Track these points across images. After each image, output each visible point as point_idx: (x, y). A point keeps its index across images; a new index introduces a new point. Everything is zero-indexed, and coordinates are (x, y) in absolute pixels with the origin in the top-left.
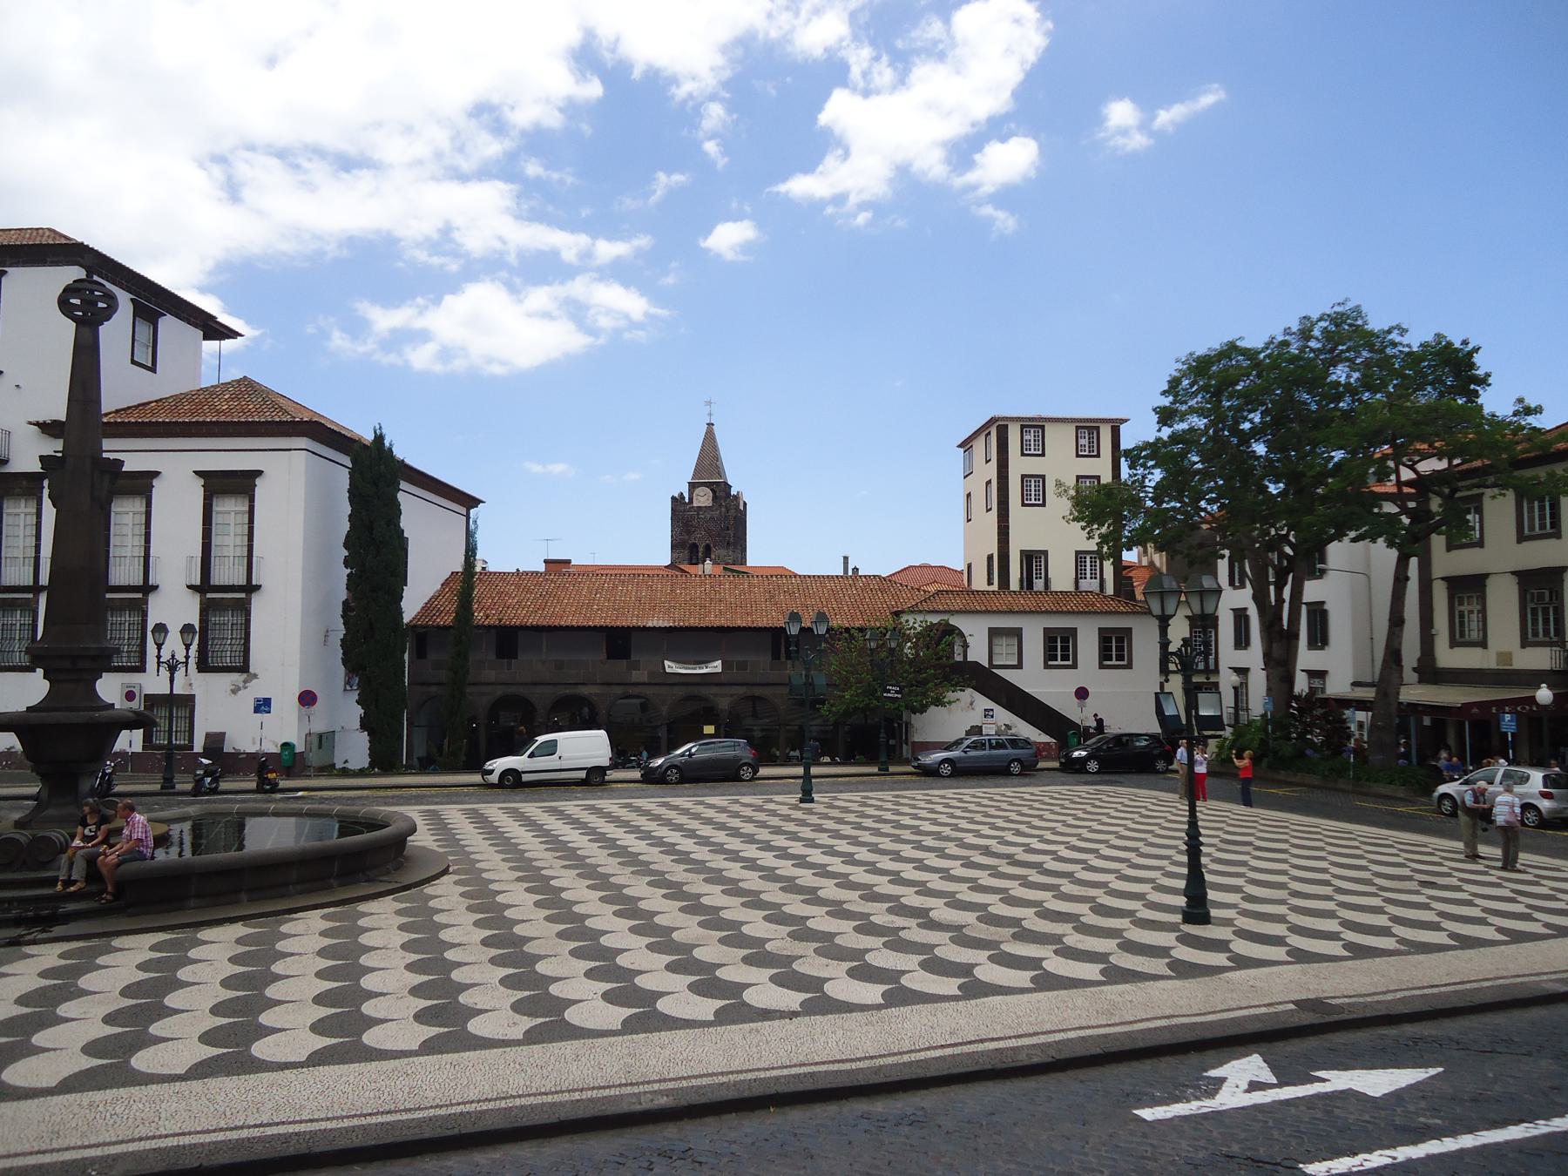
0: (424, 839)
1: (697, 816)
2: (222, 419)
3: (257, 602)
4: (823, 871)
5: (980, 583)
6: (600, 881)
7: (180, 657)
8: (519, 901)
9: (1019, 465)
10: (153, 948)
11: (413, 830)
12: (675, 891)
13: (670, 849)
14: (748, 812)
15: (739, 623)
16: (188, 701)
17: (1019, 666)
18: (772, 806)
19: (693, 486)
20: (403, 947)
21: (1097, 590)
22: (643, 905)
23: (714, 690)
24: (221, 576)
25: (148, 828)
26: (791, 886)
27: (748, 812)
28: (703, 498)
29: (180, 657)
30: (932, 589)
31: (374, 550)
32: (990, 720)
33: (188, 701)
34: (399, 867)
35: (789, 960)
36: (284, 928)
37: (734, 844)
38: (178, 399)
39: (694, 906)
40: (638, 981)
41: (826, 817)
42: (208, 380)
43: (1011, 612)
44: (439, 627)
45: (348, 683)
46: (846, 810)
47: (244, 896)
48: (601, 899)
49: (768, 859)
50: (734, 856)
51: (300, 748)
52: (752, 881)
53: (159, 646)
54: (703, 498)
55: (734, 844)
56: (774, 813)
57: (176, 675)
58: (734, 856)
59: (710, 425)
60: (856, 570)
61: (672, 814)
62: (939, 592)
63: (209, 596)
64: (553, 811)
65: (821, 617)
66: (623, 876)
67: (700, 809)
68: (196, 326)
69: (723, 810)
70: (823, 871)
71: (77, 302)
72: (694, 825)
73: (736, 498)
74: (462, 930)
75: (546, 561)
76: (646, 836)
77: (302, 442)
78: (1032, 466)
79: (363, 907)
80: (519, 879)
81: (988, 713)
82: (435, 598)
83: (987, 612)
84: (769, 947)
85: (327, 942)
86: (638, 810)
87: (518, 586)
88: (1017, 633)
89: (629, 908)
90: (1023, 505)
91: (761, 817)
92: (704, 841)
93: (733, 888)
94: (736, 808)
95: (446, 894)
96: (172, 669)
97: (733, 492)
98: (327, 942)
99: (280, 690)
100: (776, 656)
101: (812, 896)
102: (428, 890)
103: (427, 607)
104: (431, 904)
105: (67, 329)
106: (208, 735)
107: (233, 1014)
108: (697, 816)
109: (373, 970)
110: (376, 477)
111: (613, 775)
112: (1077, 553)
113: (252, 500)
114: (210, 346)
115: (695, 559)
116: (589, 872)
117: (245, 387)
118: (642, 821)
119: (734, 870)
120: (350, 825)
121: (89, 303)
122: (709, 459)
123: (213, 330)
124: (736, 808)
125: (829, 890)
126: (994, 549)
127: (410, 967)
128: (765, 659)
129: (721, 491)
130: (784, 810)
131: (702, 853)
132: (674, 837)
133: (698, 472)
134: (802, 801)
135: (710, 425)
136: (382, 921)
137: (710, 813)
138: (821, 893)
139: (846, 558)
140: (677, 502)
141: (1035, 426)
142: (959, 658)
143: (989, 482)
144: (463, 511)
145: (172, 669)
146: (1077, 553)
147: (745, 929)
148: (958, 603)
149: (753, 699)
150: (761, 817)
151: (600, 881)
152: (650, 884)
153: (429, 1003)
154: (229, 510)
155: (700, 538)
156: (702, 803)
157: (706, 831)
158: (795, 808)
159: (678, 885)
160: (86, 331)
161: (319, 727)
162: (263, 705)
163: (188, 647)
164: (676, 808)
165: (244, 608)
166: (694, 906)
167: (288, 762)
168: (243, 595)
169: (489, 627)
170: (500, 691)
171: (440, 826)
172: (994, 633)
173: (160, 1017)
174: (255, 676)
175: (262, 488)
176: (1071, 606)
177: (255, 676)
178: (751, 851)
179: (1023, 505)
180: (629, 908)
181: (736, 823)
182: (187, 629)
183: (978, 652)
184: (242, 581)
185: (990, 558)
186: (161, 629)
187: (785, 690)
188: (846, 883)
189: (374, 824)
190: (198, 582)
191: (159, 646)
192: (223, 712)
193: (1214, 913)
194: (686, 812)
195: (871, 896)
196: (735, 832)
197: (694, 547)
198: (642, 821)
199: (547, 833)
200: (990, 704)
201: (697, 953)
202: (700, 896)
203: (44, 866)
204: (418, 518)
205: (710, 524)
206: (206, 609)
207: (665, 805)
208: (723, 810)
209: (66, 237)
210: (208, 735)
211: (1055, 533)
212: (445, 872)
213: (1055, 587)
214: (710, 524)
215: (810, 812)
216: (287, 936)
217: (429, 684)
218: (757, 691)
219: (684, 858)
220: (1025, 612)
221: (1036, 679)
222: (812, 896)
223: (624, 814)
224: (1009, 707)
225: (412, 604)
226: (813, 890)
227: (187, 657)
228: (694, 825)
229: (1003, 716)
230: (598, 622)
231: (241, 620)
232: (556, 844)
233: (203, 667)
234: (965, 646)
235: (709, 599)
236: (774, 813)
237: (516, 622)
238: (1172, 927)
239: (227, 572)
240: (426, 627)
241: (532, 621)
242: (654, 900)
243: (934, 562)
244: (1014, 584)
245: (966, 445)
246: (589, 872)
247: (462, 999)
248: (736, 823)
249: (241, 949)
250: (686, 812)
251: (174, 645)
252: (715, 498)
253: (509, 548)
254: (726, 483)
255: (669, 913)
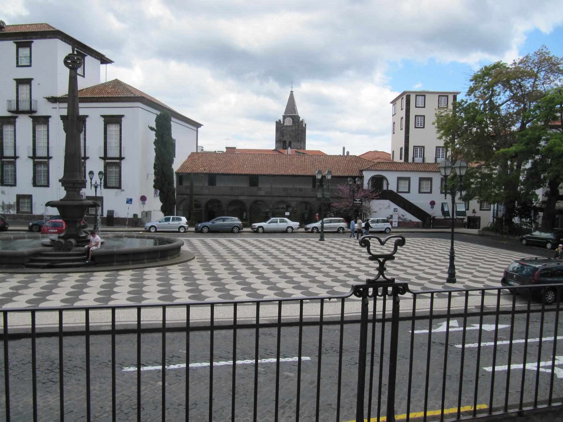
0: (185, 248)
1: (281, 244)
2: (110, 96)
3: (18, 161)
4: (324, 263)
5: (397, 159)
6: (246, 263)
7: (99, 183)
8: (219, 268)
9: (414, 112)
10: (106, 276)
11: (183, 244)
12: (272, 267)
13: (271, 254)
14: (300, 243)
15: (300, 174)
16: (101, 199)
17: (409, 192)
18: (308, 242)
19: (284, 117)
20: (183, 279)
21: (422, 162)
22: (260, 271)
23: (289, 199)
24: (111, 154)
25: (97, 242)
26: (312, 267)
27: (300, 243)
28: (289, 122)
29: (99, 183)
30: (376, 161)
31: (164, 146)
32: (396, 213)
33: (101, 199)
34: (179, 256)
35: (307, 288)
36: (145, 272)
37: (294, 254)
38: (94, 88)
39: (278, 271)
40: (258, 292)
41: (328, 246)
42: (103, 81)
43: (407, 171)
44: (187, 173)
45: (155, 193)
46: (336, 244)
47: (131, 262)
48: (246, 268)
49: (305, 259)
50: (293, 257)
51: (140, 216)
52: (298, 265)
53: (91, 179)
54: (289, 122)
55: (294, 254)
56: (309, 244)
57: (97, 189)
58: (293, 257)
59: (292, 92)
60: (348, 153)
61: (272, 243)
62: (378, 163)
63: (107, 161)
64: (230, 241)
65: (330, 172)
66: (253, 262)
67: (283, 242)
68: (98, 59)
69: (291, 242)
70: (324, 263)
71: (70, 61)
72: (280, 247)
73: (302, 122)
74: (201, 276)
75: (226, 148)
76: (263, 250)
77: (139, 104)
78: (420, 112)
79: (169, 267)
80: (219, 261)
81: (395, 210)
82: (186, 162)
83: (397, 171)
84: (301, 284)
85: (158, 277)
86: (260, 241)
87: (216, 158)
88: (408, 179)
89: (256, 271)
90: (415, 127)
91: (305, 245)
92: (283, 252)
93: (292, 267)
94: (296, 242)
95: (195, 265)
96: (96, 187)
97: (301, 119)
98: (158, 277)
99: (134, 195)
100: (314, 186)
101: (319, 270)
102: (189, 263)
103: (183, 166)
104: (190, 267)
105: (66, 71)
106: (109, 211)
107: (135, 294)
108: (281, 244)
109: (174, 285)
110: (165, 119)
111: (245, 229)
112: (437, 147)
113: (121, 126)
114: (103, 67)
115: (285, 148)
116: (242, 260)
117: (117, 83)
118: (262, 245)
119: (292, 261)
120: (162, 241)
121: (74, 62)
122: (291, 105)
123: (104, 60)
124: (296, 242)
125: (325, 268)
126: (403, 146)
127: (186, 285)
128: (310, 187)
129: (296, 119)
130: (313, 243)
131: (282, 256)
132: (273, 251)
133: (286, 111)
134: (320, 240)
135: (292, 92)
136: (175, 272)
137: (286, 243)
138: (322, 270)
139: (344, 149)
140: (278, 124)
141: (423, 94)
142: (385, 188)
143: (402, 118)
144: (195, 129)
145: (96, 187)
146: (437, 147)
147: (294, 279)
148: (386, 167)
149: (306, 203)
150: (305, 245)
151: (246, 263)
152: (263, 264)
153: (192, 294)
154: (113, 129)
155: (287, 138)
156: (283, 240)
157: (284, 249)
158: (317, 242)
159: (273, 265)
160: (73, 71)
161: (146, 209)
162: (129, 201)
163: (101, 179)
164: (274, 241)
165: (119, 165)
166: (278, 271)
167: (135, 222)
168: (118, 161)
169: (206, 174)
170: (210, 198)
171: (191, 244)
172: (399, 179)
173: (113, 294)
174: (123, 190)
175: (124, 121)
176: (431, 169)
177: (123, 190)
178: (299, 256)
179: (415, 127)
180: (256, 271)
181: (295, 247)
182: (100, 173)
183: (393, 187)
184: (118, 156)
185: (401, 149)
186: (91, 173)
187: (315, 199)
188: (331, 267)
189: (169, 241)
190: (103, 156)
191: (91, 179)
192: (114, 203)
193: (457, 280)
194: (277, 243)
195: (339, 271)
196: (294, 250)
197: (285, 142)
198: (262, 245)
199: (228, 248)
200: (396, 206)
201: (277, 285)
202: (280, 269)
203: (69, 250)
204: (178, 131)
205: (291, 132)
206: (106, 165)
207: (270, 240)
208: (291, 242)
209: (53, 28)
210: (109, 211)
211: (429, 139)
212: (194, 258)
213: (427, 161)
214: (291, 132)
215: (323, 244)
216: (146, 275)
217: (184, 195)
218: (307, 200)
219: (275, 257)
220: (412, 171)
221: (414, 198)
222: (319, 270)
223: (255, 243)
224: (404, 208)
225: (176, 166)
226: (319, 269)
227: (101, 183)
228: (280, 247)
229: (401, 211)
230: (247, 172)
231: (118, 170)
232: (231, 252)
233: (106, 187)
234: (388, 184)
235: (289, 164)
236: (309, 244)
237: (215, 172)
238: (443, 284)
239: (113, 153)
240: (183, 173)
241: (222, 171)
242: (264, 269)
243: (372, 150)
244: (410, 160)
245: (394, 102)
246: (242, 260)
247: (203, 293)
248: (295, 247)
249: (133, 277)
250: (277, 243)
251: (96, 179)
252: (293, 122)
253: (212, 141)
254: (298, 116)
255: (269, 273)
